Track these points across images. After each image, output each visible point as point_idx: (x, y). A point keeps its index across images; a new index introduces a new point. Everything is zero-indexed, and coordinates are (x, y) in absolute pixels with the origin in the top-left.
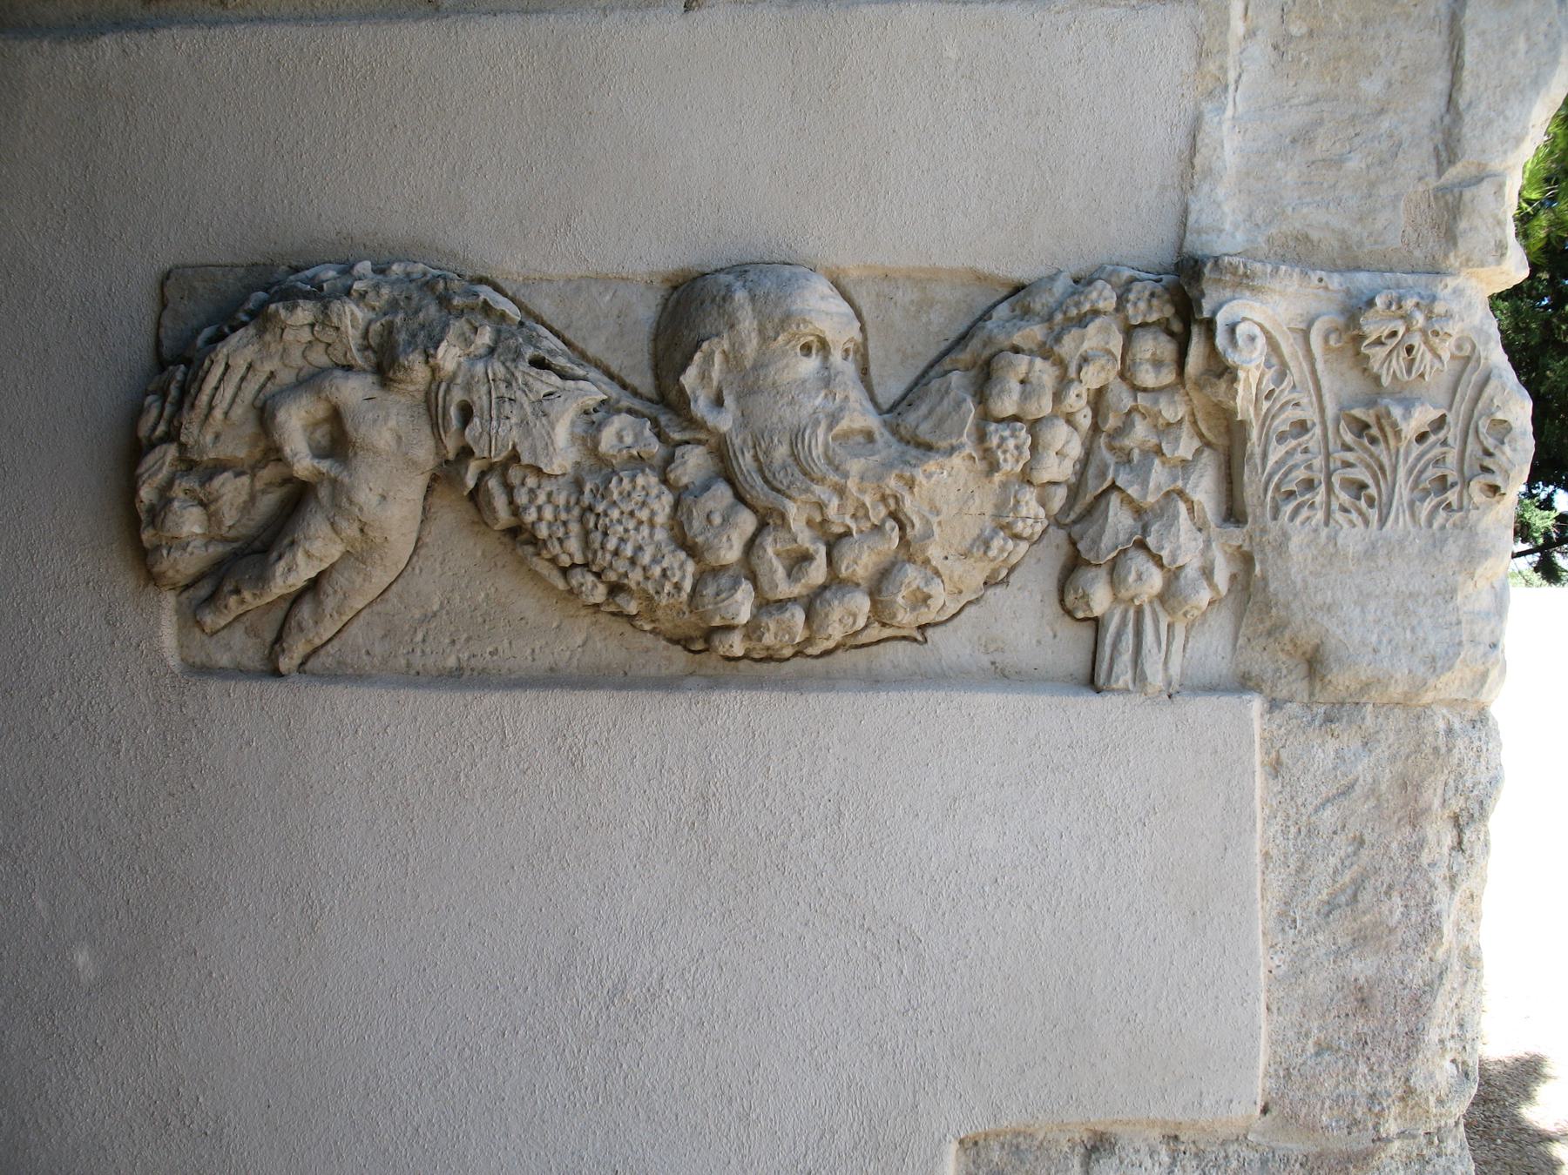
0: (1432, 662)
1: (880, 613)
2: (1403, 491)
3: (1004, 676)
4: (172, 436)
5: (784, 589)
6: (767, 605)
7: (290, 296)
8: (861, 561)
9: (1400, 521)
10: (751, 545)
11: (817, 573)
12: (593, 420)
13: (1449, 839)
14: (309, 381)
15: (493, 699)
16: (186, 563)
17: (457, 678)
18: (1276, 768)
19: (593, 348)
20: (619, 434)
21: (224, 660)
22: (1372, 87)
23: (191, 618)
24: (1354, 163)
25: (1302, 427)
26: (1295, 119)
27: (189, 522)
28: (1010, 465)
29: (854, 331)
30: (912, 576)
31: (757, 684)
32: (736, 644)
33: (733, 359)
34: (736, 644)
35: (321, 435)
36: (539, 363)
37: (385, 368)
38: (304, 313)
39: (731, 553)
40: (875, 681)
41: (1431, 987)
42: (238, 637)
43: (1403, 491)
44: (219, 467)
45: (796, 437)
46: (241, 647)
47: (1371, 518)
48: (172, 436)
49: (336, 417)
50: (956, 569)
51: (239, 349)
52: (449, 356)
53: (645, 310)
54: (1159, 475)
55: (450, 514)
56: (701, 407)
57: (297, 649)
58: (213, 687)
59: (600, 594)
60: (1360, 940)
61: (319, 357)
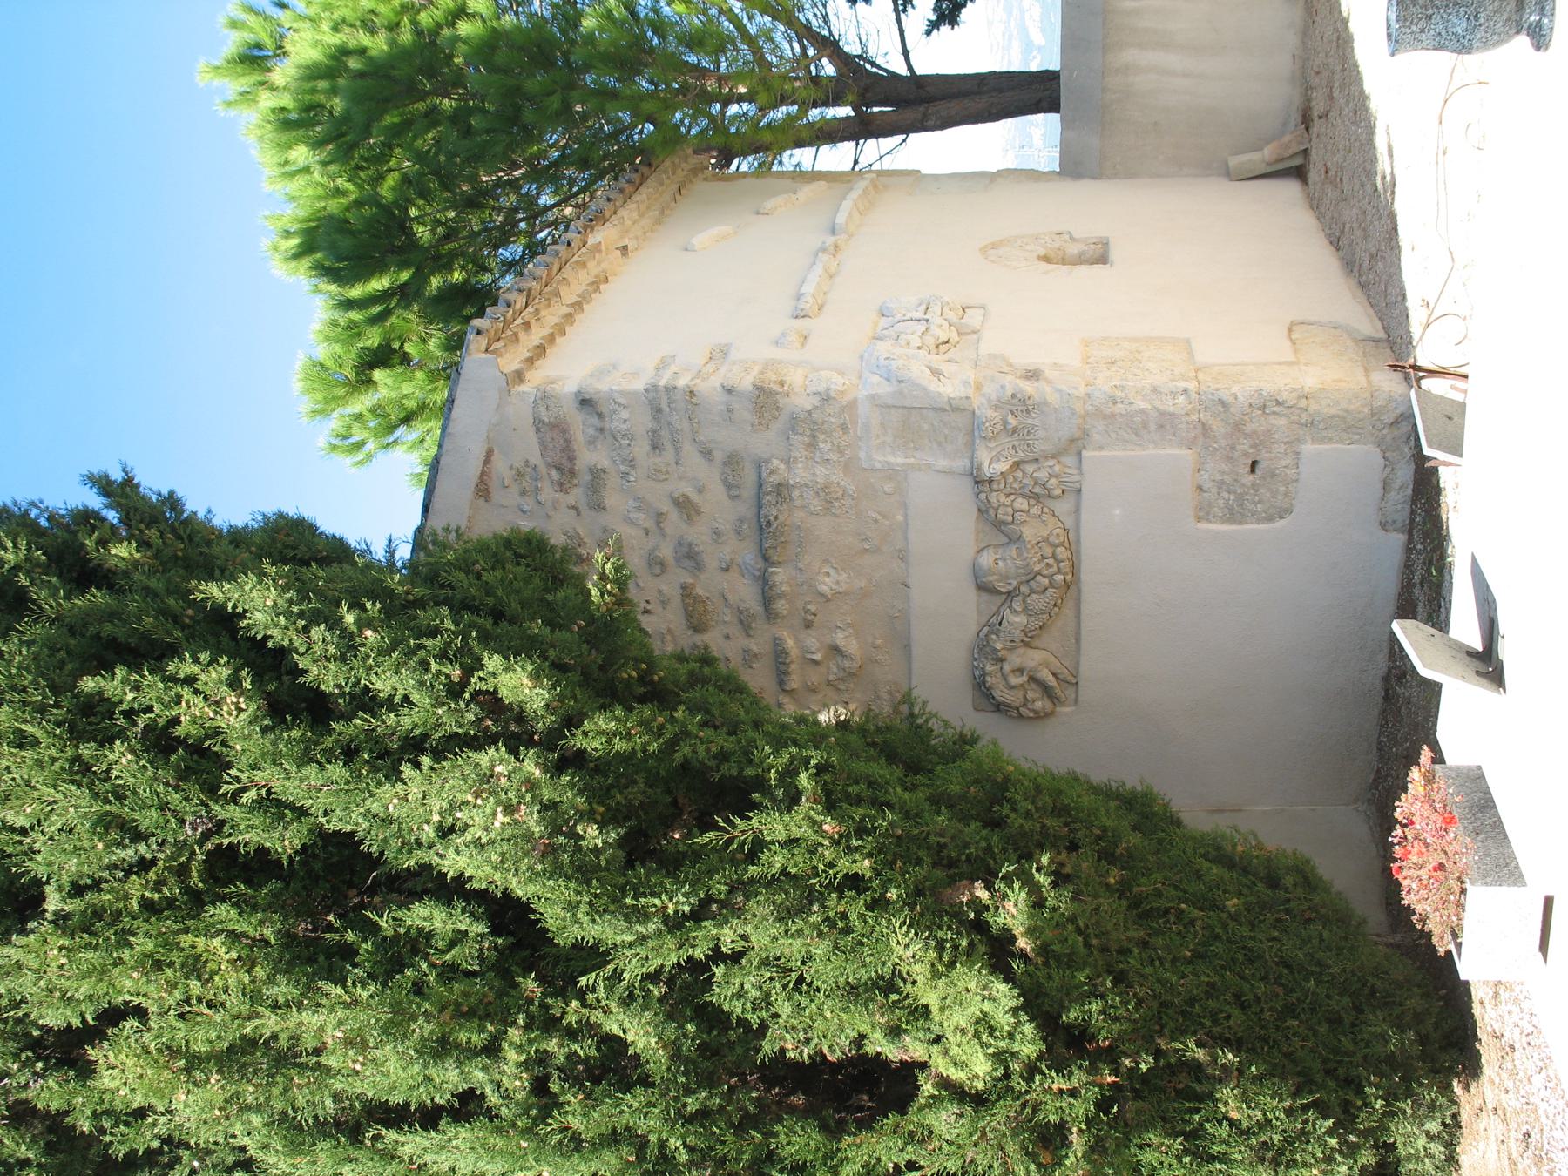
0: (1073, 414)
1: (1061, 544)
2: (1029, 421)
3: (1077, 510)
4: (1018, 709)
5: (1055, 568)
6: (1059, 571)
7: (984, 682)
8: (1048, 551)
9: (1037, 422)
10: (1044, 576)
11: (1051, 561)
12: (1014, 612)
13: (1119, 405)
14: (1005, 678)
15: (1083, 632)
16: (1049, 706)
17: (1078, 640)
18: (1101, 448)
19: (995, 609)
20: (1017, 606)
21: (1073, 696)
22: (926, 427)
23: (1063, 704)
24: (946, 431)
25: (1014, 447)
26: (935, 446)
27: (1039, 705)
28: (1024, 517)
29: (991, 550)
30: (1052, 539)
31: (1079, 570)
32: (1069, 577)
33: (998, 581)
34: (1069, 577)
35: (1017, 674)
36: (1000, 624)
37: (1002, 660)
38: (988, 679)
39: (1046, 581)
40: (1078, 541)
41: (1158, 410)
42: (1067, 692)
43: (1029, 421)
44: (1025, 697)
45: (1017, 568)
46: (1070, 692)
47: (1028, 383)
48: (1018, 709)
49: (1013, 671)
50: (1050, 527)
51: (997, 694)
52: (999, 646)
53: (985, 596)
54: (1026, 481)
55: (1036, 643)
56: (1011, 588)
57: (1070, 678)
58: (1080, 698)
59: (1057, 609)
60: (1145, 427)
61: (999, 675)
